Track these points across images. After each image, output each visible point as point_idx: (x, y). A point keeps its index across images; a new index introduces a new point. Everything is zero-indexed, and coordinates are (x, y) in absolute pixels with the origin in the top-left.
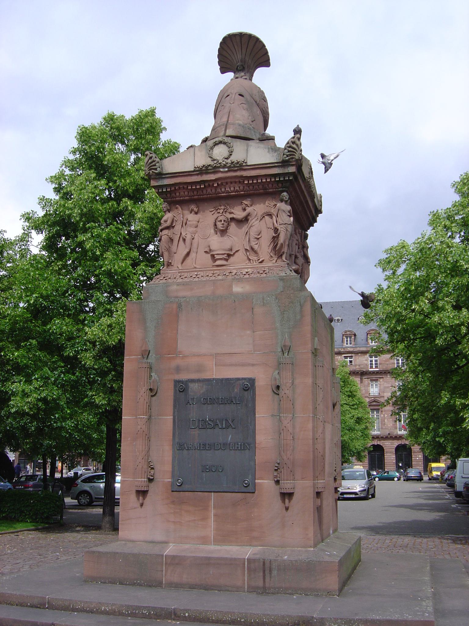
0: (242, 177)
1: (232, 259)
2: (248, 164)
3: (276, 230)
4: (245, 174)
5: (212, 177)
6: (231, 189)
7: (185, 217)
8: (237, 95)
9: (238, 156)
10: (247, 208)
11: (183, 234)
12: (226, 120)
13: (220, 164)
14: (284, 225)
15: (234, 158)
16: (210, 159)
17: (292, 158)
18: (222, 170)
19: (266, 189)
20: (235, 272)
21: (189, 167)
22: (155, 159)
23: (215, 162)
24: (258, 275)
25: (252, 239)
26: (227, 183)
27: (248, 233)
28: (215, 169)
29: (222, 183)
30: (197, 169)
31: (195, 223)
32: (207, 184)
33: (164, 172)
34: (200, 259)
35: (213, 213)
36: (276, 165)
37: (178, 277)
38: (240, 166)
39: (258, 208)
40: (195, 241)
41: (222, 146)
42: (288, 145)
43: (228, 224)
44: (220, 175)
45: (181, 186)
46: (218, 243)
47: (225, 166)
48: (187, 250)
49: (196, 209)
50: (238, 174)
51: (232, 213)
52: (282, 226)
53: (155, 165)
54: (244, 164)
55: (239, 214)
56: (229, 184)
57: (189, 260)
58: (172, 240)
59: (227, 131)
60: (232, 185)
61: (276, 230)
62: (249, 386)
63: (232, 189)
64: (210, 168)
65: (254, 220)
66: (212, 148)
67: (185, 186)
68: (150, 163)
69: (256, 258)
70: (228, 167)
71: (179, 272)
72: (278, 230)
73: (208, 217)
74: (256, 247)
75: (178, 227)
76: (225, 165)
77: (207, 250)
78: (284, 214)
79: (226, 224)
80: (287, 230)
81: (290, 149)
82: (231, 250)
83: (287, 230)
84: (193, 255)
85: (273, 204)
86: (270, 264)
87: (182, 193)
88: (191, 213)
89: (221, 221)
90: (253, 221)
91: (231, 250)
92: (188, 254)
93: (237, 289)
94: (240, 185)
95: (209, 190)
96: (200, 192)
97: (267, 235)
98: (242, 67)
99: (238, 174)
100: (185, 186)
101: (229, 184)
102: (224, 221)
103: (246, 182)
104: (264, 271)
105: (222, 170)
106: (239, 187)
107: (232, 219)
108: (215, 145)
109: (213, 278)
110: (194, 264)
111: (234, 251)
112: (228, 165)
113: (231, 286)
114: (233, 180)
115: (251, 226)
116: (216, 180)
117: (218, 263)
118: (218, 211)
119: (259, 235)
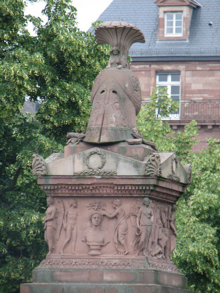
0: (112, 184)
1: (104, 249)
2: (118, 175)
3: (138, 230)
4: (115, 182)
5: (89, 182)
6: (104, 191)
7: (66, 211)
8: (111, 92)
9: (109, 167)
10: (116, 207)
11: (65, 225)
12: (101, 123)
13: (95, 172)
14: (145, 227)
15: (106, 168)
16: (86, 167)
17: (152, 174)
18: (96, 177)
19: (132, 194)
20: (106, 261)
21: (70, 173)
22: (41, 162)
23: (91, 170)
24: (124, 267)
25: (119, 235)
26: (100, 187)
27: (117, 230)
28: (91, 176)
29: (96, 187)
30: (76, 174)
31: (74, 216)
32: (84, 187)
33: (48, 174)
34: (79, 246)
35: (90, 208)
36: (139, 177)
37: (60, 263)
38: (111, 176)
39: (127, 206)
40: (74, 232)
41: (96, 155)
42: (149, 162)
43: (101, 220)
44: (95, 181)
45: (63, 186)
46: (93, 236)
47: (98, 175)
48: (68, 239)
49: (75, 205)
50: (109, 181)
51: (104, 210)
52: (143, 227)
53: (41, 167)
54: (114, 175)
55: (110, 211)
56: (102, 188)
57: (69, 248)
58: (55, 229)
59: (102, 137)
60: (104, 189)
61: (138, 230)
62: (179, 86)
63: (105, 191)
64: (86, 174)
65: (121, 219)
66: (88, 158)
67: (66, 187)
68: (37, 165)
69: (122, 250)
70: (102, 176)
71: (61, 258)
72: (140, 230)
73: (86, 209)
74: (123, 242)
75: (60, 218)
76: (99, 174)
77: (84, 239)
78: (145, 217)
79: (100, 220)
80: (147, 230)
81: (150, 166)
82: (103, 242)
83: (147, 230)
84: (73, 243)
85: (137, 206)
86: (133, 257)
87: (64, 191)
88: (71, 206)
89: (95, 218)
90: (121, 220)
91: (103, 242)
92: (69, 242)
93: (107, 277)
94: (111, 189)
95: (86, 191)
96: (78, 192)
97: (131, 233)
98: (117, 52)
99: (109, 181)
100: (66, 187)
101: (102, 188)
102: (98, 218)
103: (116, 188)
104: (128, 263)
105: (96, 177)
106: (110, 191)
107: (104, 216)
108: (91, 155)
109: (88, 267)
110: (73, 251)
111: (105, 243)
112: (101, 174)
113: (102, 276)
114: (105, 186)
115: (119, 224)
116: (91, 184)
117: (93, 252)
118: (93, 207)
119: (125, 231)
